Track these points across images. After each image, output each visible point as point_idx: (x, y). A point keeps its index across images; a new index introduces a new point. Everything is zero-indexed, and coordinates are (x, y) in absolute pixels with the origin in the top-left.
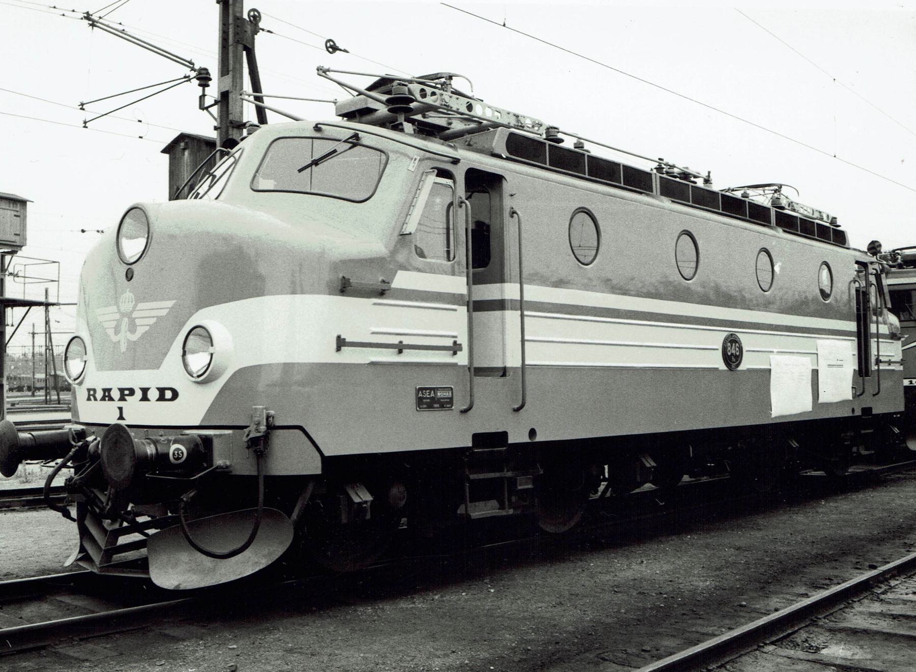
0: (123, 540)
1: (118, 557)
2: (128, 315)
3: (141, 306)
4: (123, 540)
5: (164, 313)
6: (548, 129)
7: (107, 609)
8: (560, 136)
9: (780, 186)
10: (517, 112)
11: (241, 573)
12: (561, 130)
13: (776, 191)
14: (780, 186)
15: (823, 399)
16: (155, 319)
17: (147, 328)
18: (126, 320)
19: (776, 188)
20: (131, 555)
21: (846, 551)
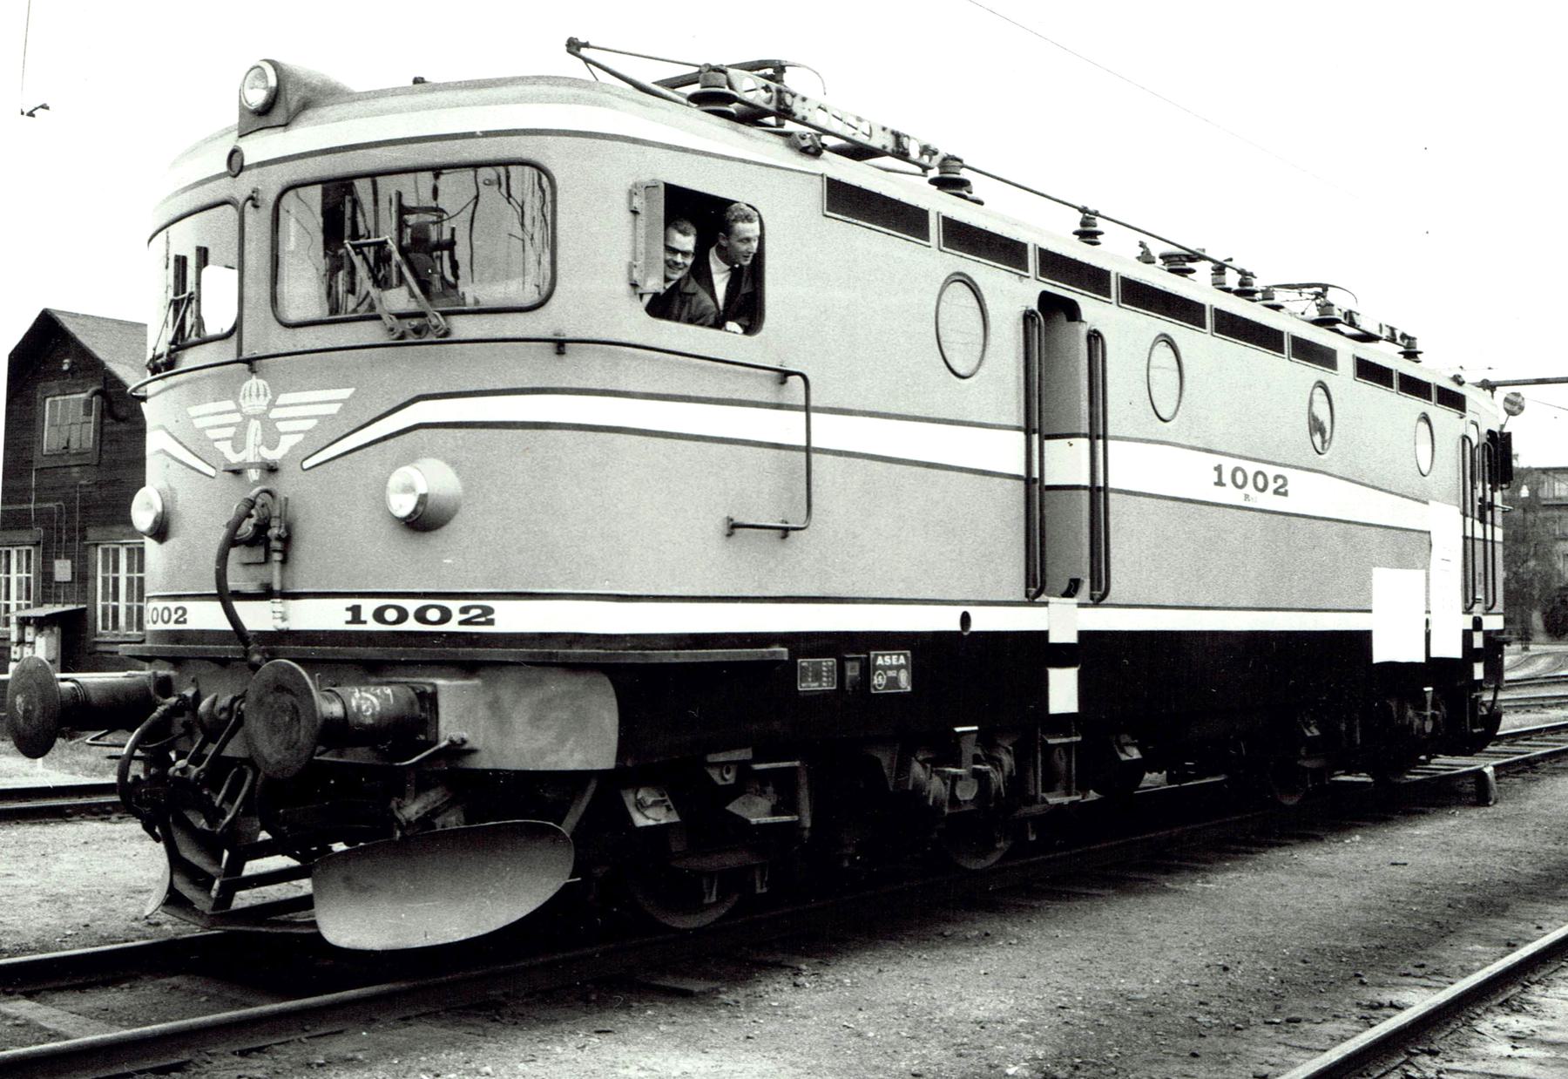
0: (253, 867)
1: (244, 899)
2: (263, 418)
3: (283, 399)
4: (253, 867)
5: (334, 409)
6: (944, 159)
7: (233, 1005)
8: (964, 174)
9: (780, 69)
10: (901, 130)
11: (542, 753)
12: (966, 162)
13: (1318, 295)
14: (1325, 287)
15: (1434, 654)
16: (315, 422)
17: (300, 437)
18: (255, 425)
19: (1320, 290)
20: (274, 892)
21: (1488, 904)
